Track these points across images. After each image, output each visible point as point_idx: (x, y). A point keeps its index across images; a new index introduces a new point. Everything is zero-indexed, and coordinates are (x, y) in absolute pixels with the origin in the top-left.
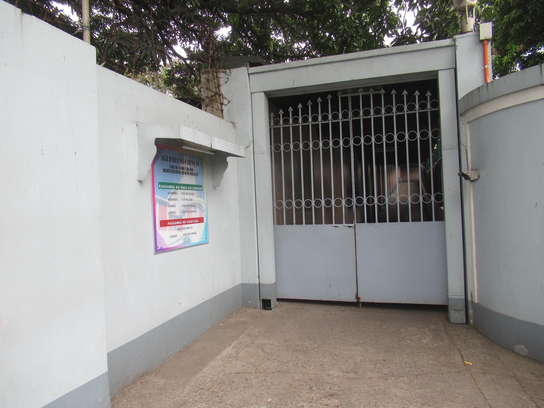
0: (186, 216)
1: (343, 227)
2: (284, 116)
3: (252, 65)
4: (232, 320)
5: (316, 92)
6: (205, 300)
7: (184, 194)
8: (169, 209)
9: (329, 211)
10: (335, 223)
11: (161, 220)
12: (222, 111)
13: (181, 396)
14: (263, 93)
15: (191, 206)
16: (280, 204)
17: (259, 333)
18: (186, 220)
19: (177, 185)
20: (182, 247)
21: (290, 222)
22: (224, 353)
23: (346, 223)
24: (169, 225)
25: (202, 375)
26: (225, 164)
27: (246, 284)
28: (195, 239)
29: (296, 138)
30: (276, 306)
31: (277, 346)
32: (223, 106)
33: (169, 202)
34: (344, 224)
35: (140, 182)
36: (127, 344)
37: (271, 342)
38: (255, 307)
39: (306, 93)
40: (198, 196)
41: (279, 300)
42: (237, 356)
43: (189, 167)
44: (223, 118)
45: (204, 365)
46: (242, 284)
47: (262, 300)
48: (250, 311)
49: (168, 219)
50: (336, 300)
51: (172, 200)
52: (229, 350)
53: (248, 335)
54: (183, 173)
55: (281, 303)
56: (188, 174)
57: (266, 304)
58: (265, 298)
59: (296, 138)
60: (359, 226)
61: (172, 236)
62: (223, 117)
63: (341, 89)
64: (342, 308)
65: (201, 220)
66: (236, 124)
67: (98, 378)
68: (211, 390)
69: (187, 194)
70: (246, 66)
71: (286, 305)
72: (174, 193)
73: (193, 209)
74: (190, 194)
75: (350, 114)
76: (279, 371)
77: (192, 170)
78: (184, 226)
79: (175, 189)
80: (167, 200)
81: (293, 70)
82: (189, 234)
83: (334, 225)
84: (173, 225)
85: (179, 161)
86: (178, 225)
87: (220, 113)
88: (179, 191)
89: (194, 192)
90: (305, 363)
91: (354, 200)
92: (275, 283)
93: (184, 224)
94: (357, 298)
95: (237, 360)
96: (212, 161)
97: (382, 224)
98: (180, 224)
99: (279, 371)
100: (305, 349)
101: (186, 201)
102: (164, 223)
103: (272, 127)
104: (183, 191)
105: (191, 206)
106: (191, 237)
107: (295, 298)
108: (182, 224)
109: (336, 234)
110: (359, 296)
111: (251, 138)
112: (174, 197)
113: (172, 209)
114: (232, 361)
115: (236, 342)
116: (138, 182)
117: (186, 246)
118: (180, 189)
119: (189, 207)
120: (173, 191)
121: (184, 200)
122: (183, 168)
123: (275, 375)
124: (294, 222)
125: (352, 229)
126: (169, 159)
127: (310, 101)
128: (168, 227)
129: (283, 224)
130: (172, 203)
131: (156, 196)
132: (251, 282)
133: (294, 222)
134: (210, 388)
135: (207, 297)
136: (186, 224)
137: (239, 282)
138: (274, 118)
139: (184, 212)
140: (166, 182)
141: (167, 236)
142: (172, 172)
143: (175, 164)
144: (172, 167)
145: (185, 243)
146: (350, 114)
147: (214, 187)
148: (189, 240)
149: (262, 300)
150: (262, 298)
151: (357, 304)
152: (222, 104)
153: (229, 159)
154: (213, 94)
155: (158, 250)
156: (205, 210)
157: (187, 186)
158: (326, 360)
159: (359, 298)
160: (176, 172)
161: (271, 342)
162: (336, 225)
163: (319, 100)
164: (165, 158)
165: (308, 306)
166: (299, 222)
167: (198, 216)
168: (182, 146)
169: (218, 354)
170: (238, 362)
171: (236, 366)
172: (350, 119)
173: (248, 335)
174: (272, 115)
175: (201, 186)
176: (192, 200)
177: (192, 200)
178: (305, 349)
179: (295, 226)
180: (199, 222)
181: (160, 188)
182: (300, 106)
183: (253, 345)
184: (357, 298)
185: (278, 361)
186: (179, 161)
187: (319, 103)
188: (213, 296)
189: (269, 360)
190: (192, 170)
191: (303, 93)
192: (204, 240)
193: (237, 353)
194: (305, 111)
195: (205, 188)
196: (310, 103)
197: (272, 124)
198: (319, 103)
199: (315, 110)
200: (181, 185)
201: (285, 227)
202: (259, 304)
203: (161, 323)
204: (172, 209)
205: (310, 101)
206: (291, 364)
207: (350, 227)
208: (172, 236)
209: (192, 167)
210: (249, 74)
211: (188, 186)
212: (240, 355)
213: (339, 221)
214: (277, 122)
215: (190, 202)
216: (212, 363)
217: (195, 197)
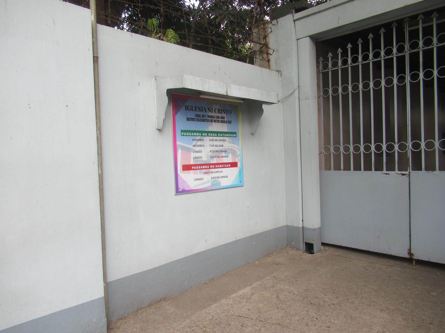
0: (215, 161)
1: (395, 175)
2: (332, 58)
3: (297, 11)
4: (269, 260)
5: (366, 27)
6: (238, 238)
7: (213, 140)
8: (193, 155)
9: (390, 156)
10: (387, 170)
11: (184, 164)
12: (269, 61)
13: (176, 329)
14: (308, 38)
15: (222, 151)
16: (327, 149)
17: (286, 277)
18: (215, 164)
19: (205, 132)
20: (209, 189)
21: (337, 168)
22: (241, 292)
23: (399, 170)
24: (194, 169)
25: (207, 311)
26: (261, 111)
27: (290, 226)
28: (224, 183)
29: (345, 81)
30: (320, 251)
31: (294, 294)
32: (269, 55)
33: (194, 148)
34: (397, 171)
35: (159, 130)
36: (148, 270)
37: (292, 289)
38: (298, 249)
39: (354, 31)
40: (230, 143)
41: (323, 244)
42: (250, 298)
43: (220, 115)
44: (269, 69)
45: (215, 301)
46: (287, 226)
47: (306, 243)
48: (292, 252)
49: (192, 163)
50: (385, 252)
51: (197, 146)
52: (247, 290)
53: (275, 277)
54: (211, 121)
55: (327, 248)
56: (218, 121)
57: (309, 248)
58: (308, 242)
59: (345, 81)
60: (415, 174)
61: (197, 179)
62: (269, 67)
63: (396, 19)
64: (392, 262)
65: (234, 165)
66: (283, 72)
67: (93, 302)
68: (204, 329)
69: (216, 140)
70: (292, 13)
71: (331, 250)
72: (200, 140)
73: (224, 154)
74: (220, 140)
75: (407, 46)
76: (279, 324)
77: (224, 118)
78: (211, 170)
79: (202, 135)
80: (191, 147)
81: (338, 8)
82: (217, 178)
83: (385, 171)
84: (199, 169)
85: (207, 110)
86: (205, 169)
87: (267, 64)
88: (207, 138)
89: (225, 138)
90: (312, 321)
91: (373, 147)
92: (320, 228)
93: (213, 168)
94: (410, 253)
95: (247, 302)
96: (248, 110)
97: (430, 174)
98: (207, 169)
99: (279, 324)
100: (322, 303)
101: (215, 147)
102: (187, 168)
103: (321, 71)
104: (211, 138)
105: (222, 151)
106: (221, 180)
107: (341, 245)
108: (210, 168)
109: (390, 181)
110: (412, 252)
111: (296, 85)
112: (199, 143)
113: (198, 155)
114: (242, 302)
115: (258, 283)
116: (157, 130)
117: (213, 189)
118: (208, 136)
119: (218, 153)
120: (198, 138)
121: (213, 146)
122: (212, 117)
123: (273, 327)
124: (342, 168)
125: (406, 178)
126: (194, 109)
127: (360, 39)
128: (192, 171)
129: (330, 169)
130: (197, 149)
131: (178, 143)
132: (295, 225)
133: (342, 168)
134: (205, 327)
135: (240, 236)
136: (215, 168)
137: (283, 223)
138: (323, 62)
139: (212, 157)
140: (186, 129)
141: (189, 179)
142: (198, 120)
143: (201, 113)
144: (197, 116)
145: (212, 185)
146: (407, 46)
147: (252, 134)
148: (219, 183)
149: (306, 243)
150: (305, 241)
151: (409, 260)
152: (268, 54)
153: (264, 107)
154: (261, 46)
155: (178, 192)
156: (239, 155)
157: (217, 133)
158: (336, 322)
159: (413, 255)
160: (203, 121)
161: (292, 289)
162: (388, 172)
163: (371, 36)
164: (189, 108)
165: (353, 255)
166: (347, 168)
167: (231, 161)
168: (200, 95)
169: (235, 293)
170: (248, 304)
171: (242, 308)
172: (407, 53)
173: (275, 277)
174: (321, 59)
175: (235, 133)
176: (222, 146)
177: (222, 146)
178: (322, 303)
179: (343, 173)
180: (231, 167)
181: (183, 135)
182: (349, 46)
183: (272, 289)
184: (410, 253)
185: (286, 312)
186: (207, 110)
187: (371, 39)
188: (248, 235)
189: (277, 308)
190: (224, 118)
191: (352, 32)
192: (181, 188)
193: (252, 294)
194: (355, 51)
195: (240, 135)
196: (360, 41)
197: (321, 67)
198: (371, 39)
199: (365, 49)
200: (208, 132)
201: (333, 173)
202: (302, 247)
203: (183, 256)
204: (198, 155)
205: (360, 39)
206: (297, 318)
207: (403, 175)
208: (197, 179)
209: (224, 115)
210: (294, 21)
211: (217, 133)
212: (254, 297)
213: (390, 168)
214: (325, 66)
215: (221, 148)
216: (223, 301)
217: (227, 143)
